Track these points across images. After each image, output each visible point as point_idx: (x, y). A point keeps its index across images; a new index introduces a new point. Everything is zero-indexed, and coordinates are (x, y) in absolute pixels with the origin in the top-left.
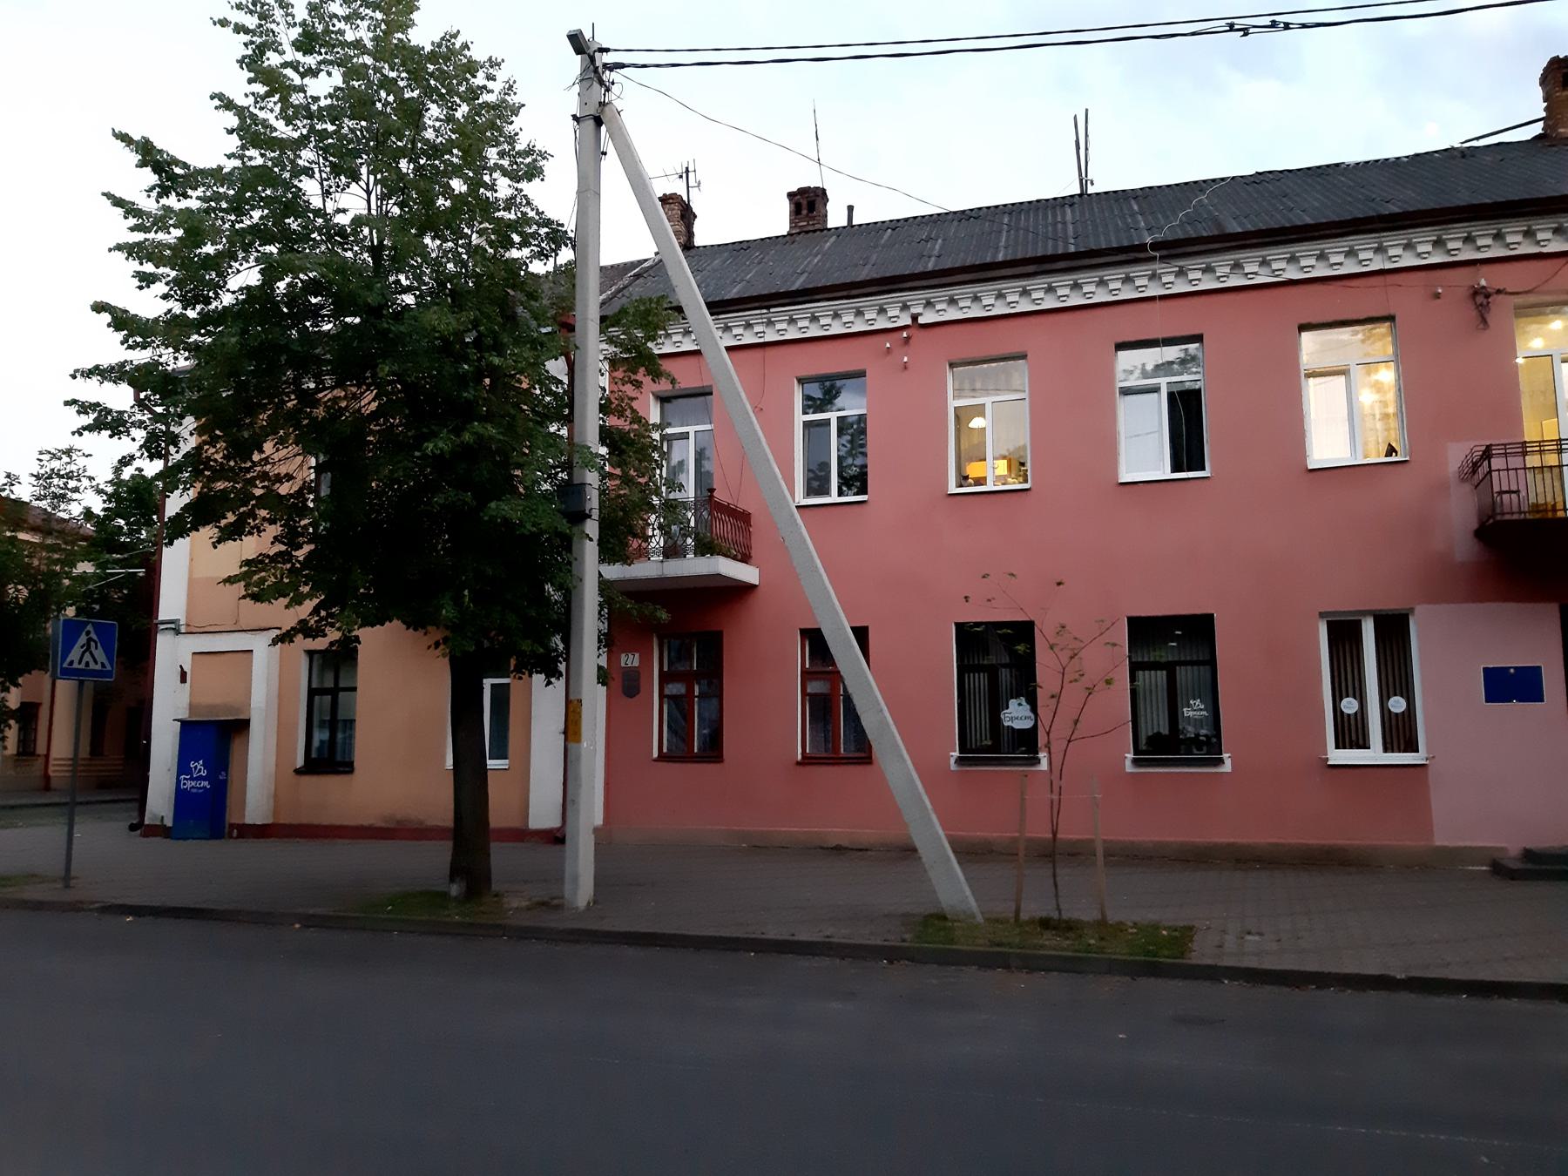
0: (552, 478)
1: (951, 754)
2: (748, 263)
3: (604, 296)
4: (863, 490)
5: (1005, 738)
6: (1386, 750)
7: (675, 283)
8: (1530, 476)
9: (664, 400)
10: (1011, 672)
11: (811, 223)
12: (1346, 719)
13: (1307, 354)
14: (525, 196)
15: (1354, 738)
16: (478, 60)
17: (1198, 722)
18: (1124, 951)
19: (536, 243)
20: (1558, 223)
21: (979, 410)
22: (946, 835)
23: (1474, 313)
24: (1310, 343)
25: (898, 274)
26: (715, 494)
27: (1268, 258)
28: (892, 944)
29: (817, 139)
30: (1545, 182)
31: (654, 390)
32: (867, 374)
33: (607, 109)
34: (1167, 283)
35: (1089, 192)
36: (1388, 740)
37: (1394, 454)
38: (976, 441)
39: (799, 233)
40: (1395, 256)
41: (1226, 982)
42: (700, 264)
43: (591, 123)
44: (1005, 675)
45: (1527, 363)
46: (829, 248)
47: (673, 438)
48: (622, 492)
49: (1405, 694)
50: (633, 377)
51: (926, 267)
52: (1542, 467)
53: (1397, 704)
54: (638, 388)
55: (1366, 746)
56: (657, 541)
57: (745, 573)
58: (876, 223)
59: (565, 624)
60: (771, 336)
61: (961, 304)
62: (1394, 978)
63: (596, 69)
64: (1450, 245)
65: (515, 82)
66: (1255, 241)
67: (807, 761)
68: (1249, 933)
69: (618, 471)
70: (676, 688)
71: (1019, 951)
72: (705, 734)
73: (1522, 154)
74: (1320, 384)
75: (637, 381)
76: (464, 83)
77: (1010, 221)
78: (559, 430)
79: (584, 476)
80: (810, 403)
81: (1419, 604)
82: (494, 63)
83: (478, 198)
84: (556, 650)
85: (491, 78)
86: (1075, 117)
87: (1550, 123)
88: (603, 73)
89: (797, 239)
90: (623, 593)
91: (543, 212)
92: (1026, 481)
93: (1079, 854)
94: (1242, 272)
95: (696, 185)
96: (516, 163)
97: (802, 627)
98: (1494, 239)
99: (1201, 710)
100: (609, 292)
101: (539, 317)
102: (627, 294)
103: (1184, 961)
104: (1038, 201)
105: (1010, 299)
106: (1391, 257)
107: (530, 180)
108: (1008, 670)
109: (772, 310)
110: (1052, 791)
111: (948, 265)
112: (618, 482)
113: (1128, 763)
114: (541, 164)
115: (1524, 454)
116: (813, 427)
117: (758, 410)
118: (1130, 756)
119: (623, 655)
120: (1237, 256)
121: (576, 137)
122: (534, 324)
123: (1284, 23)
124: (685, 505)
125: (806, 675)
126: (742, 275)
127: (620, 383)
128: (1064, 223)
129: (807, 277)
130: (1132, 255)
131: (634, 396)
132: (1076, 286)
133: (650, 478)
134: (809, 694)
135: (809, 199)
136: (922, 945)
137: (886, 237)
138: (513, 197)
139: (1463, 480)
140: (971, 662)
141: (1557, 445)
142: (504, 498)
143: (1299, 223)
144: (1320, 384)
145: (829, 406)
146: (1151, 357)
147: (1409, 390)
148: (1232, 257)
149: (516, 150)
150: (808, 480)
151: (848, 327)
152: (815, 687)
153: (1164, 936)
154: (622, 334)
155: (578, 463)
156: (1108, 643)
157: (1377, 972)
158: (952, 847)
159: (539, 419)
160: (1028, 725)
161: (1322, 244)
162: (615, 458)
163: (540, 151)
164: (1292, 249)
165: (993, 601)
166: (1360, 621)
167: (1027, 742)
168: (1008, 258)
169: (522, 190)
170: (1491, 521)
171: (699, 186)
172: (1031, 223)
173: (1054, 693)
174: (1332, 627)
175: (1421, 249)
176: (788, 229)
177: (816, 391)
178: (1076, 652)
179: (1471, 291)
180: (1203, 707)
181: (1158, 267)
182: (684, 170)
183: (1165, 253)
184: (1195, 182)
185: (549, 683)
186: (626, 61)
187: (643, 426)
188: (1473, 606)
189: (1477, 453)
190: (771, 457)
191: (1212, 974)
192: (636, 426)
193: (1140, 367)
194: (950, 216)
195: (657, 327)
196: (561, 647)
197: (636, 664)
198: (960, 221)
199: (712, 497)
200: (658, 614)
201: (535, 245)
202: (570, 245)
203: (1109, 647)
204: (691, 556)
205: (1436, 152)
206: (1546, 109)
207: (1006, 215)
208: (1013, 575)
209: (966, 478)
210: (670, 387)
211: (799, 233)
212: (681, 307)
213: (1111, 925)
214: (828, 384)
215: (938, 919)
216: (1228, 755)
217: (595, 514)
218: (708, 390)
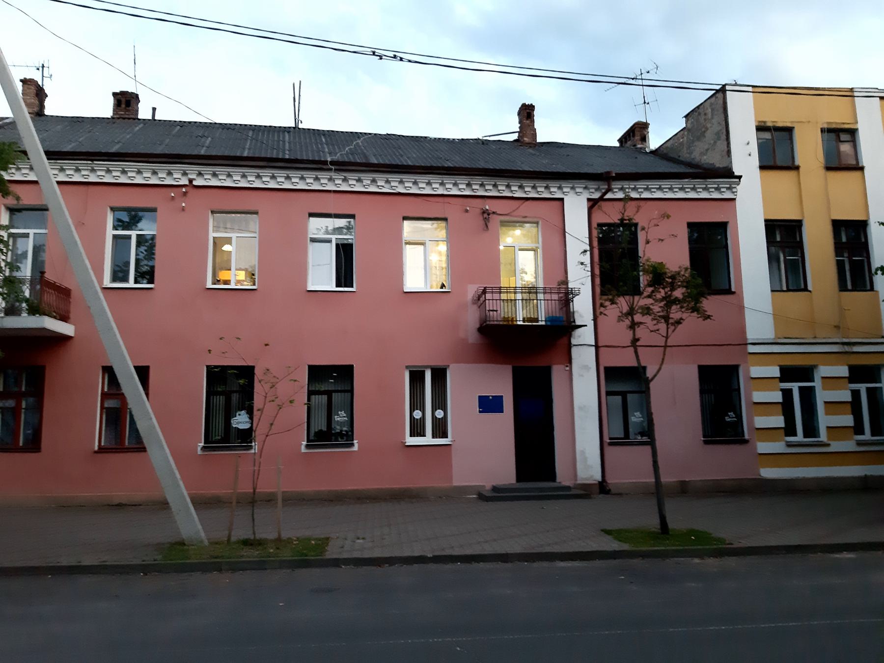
4: (151, 281)
5: (233, 434)
6: (433, 437)
7: (22, 135)
11: (127, 113)
12: (438, 420)
13: (407, 232)
15: (419, 431)
17: (341, 424)
20: (520, 183)
21: (228, 241)
22: (188, 494)
23: (482, 222)
25: (187, 153)
27: (650, 186)
28: (149, 562)
31: (5, 203)
32: (158, 211)
36: (435, 432)
37: (444, 288)
39: (118, 118)
41: (343, 567)
44: (235, 397)
46: (138, 131)
53: (440, 414)
60: (93, 178)
62: (427, 557)
64: (539, 189)
67: (102, 450)
68: (358, 539)
71: (228, 560)
77: (253, 135)
80: (120, 224)
81: (452, 363)
87: (521, 135)
89: (117, 121)
92: (254, 285)
98: (440, 185)
104: (270, 126)
106: (447, 189)
108: (238, 394)
111: (214, 153)
113: (303, 447)
115: (500, 293)
118: (305, 443)
123: (400, 57)
124: (21, 281)
125: (105, 396)
128: (284, 142)
130: (320, 166)
135: (127, 99)
136: (178, 561)
140: (212, 390)
152: (110, 403)
153: (312, 544)
156: (292, 380)
157: (419, 555)
160: (247, 426)
161: (225, 168)
164: (401, 177)
167: (246, 436)
174: (411, 373)
176: (112, 114)
178: (274, 384)
179: (482, 211)
181: (334, 175)
183: (337, 167)
184: (356, 133)
191: (336, 563)
193: (324, 228)
203: (292, 382)
204: (25, 314)
206: (520, 127)
207: (251, 131)
211: (118, 118)
212: (26, 152)
214: (133, 213)
218: (44, 207)
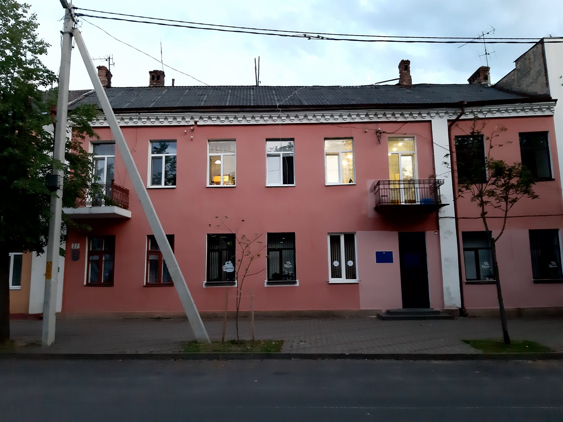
0: (44, 173)
1: (204, 282)
2: (132, 95)
3: (70, 103)
4: (174, 184)
6: (347, 278)
7: (100, 100)
8: (391, 191)
9: (95, 144)
10: (227, 252)
11: (158, 83)
14: (38, 60)
15: (337, 274)
16: (19, 4)
18: (259, 351)
19: (42, 79)
20: (446, 111)
21: (219, 158)
22: (198, 312)
23: (376, 138)
24: (328, 144)
26: (115, 182)
28: (176, 353)
29: (162, 53)
30: (399, 99)
33: (75, 30)
34: (231, 121)
35: (259, 85)
38: (217, 169)
40: (345, 118)
41: (293, 359)
42: (113, 94)
43: (68, 35)
44: (225, 253)
45: (391, 155)
46: (164, 94)
47: (97, 159)
48: (74, 179)
49: (353, 260)
50: (81, 135)
51: (201, 104)
52: (394, 189)
53: (350, 263)
54: (83, 139)
55: (341, 277)
56: (89, 199)
57: (126, 213)
58: (183, 87)
59: (46, 231)
60: (140, 124)
61: (205, 119)
63: (71, 15)
65: (36, 15)
66: (312, 108)
67: (148, 285)
68: (301, 342)
69: (73, 171)
70: (96, 258)
72: (106, 276)
73: (393, 89)
74: (330, 158)
75: (83, 136)
76: (13, 12)
77: (231, 92)
78: (47, 153)
79: (57, 172)
80: (155, 150)
82: (26, 6)
83: (17, 58)
84: (42, 242)
85: (25, 11)
86: (255, 59)
87: (401, 80)
88: (75, 16)
89: (153, 89)
90: (72, 220)
91: (46, 67)
93: (247, 316)
94: (307, 118)
95: (113, 64)
96: (35, 47)
97: (148, 234)
99: (290, 265)
100: (74, 101)
101: (42, 108)
102: (81, 102)
103: (279, 353)
104: (242, 86)
105: (230, 119)
107: (41, 54)
109: (141, 114)
110: (237, 294)
112: (73, 175)
113: (265, 284)
114: (46, 48)
115: (389, 184)
116: (156, 159)
117: (133, 151)
118: (266, 281)
119: (73, 244)
120: (306, 113)
121: (61, 40)
122: (39, 111)
124: (102, 186)
125: (149, 252)
126: (130, 100)
127: (75, 136)
128: (250, 95)
129: (155, 103)
130: (273, 109)
131: (81, 142)
132: (253, 117)
133: (86, 175)
134: (150, 260)
137: (186, 92)
138: (34, 60)
139: (371, 192)
141: (419, 181)
142: (21, 179)
143: (325, 104)
144: (330, 158)
145: (163, 151)
146: (279, 144)
147: (357, 162)
148: (296, 113)
149: (36, 41)
150: (153, 178)
151: (144, 124)
152: (152, 257)
154: (77, 118)
155: (54, 167)
158: (200, 316)
159: (39, 148)
160: (232, 271)
162: (72, 166)
163: (46, 43)
165: (219, 226)
166: (340, 236)
167: (231, 277)
168: (230, 105)
169: (37, 58)
170: (379, 205)
171: (114, 65)
172: (239, 94)
173: (240, 259)
175: (362, 116)
176: (149, 85)
177: (158, 146)
180: (555, 264)
182: (108, 58)
183: (283, 109)
184: (294, 87)
185: (38, 255)
186: (84, 14)
187: (85, 154)
188: (374, 232)
189: (375, 183)
190: (136, 169)
191: (289, 356)
192: (81, 154)
193: (275, 147)
194: (210, 88)
195: (92, 116)
196: (44, 240)
197: (78, 247)
198: (214, 90)
199: (113, 183)
200: (88, 228)
201: (41, 80)
202: (56, 81)
204: (103, 206)
205: (368, 86)
206: (400, 76)
208: (226, 217)
209: (213, 182)
210: (97, 139)
211: (153, 87)
213: (256, 341)
214: (163, 143)
215: (195, 343)
216: (298, 280)
217: (62, 187)
